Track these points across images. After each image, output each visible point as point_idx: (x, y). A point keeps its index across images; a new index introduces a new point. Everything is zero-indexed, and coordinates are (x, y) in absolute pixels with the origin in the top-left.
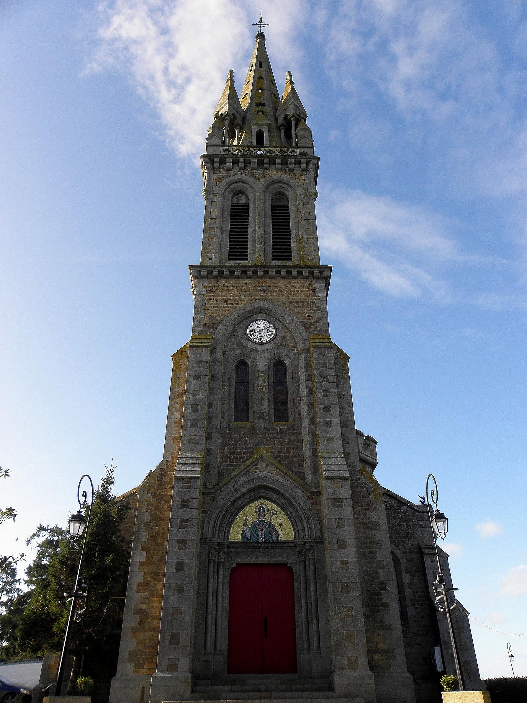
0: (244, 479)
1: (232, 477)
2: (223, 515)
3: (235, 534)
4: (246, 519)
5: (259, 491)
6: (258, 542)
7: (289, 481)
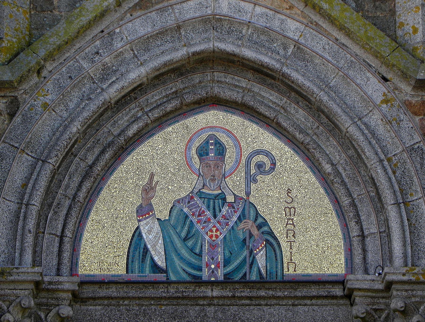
0: (140, 26)
1: (84, 20)
2: (54, 174)
3: (101, 253)
4: (149, 190)
5: (208, 75)
6: (198, 282)
7: (328, 35)
